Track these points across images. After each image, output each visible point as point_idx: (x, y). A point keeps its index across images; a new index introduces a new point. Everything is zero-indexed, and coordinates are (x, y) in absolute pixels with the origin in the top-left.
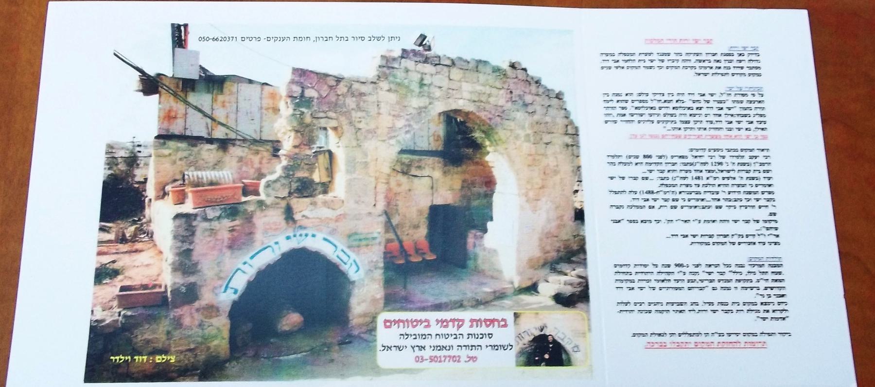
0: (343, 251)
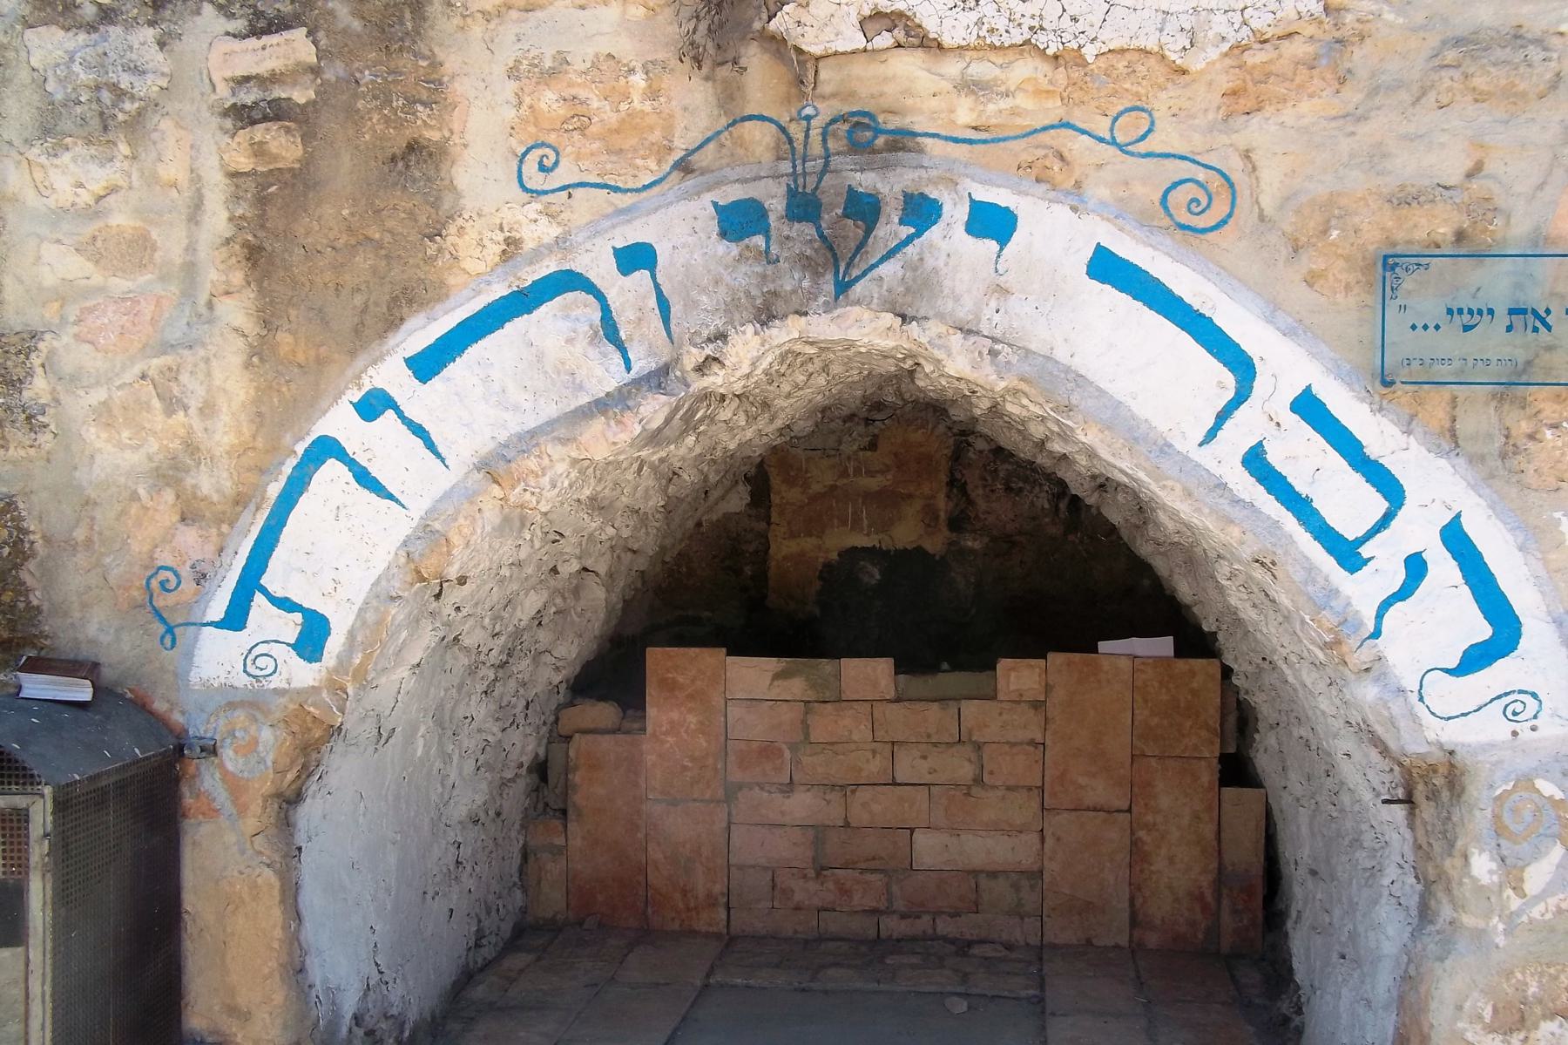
0: (1309, 407)
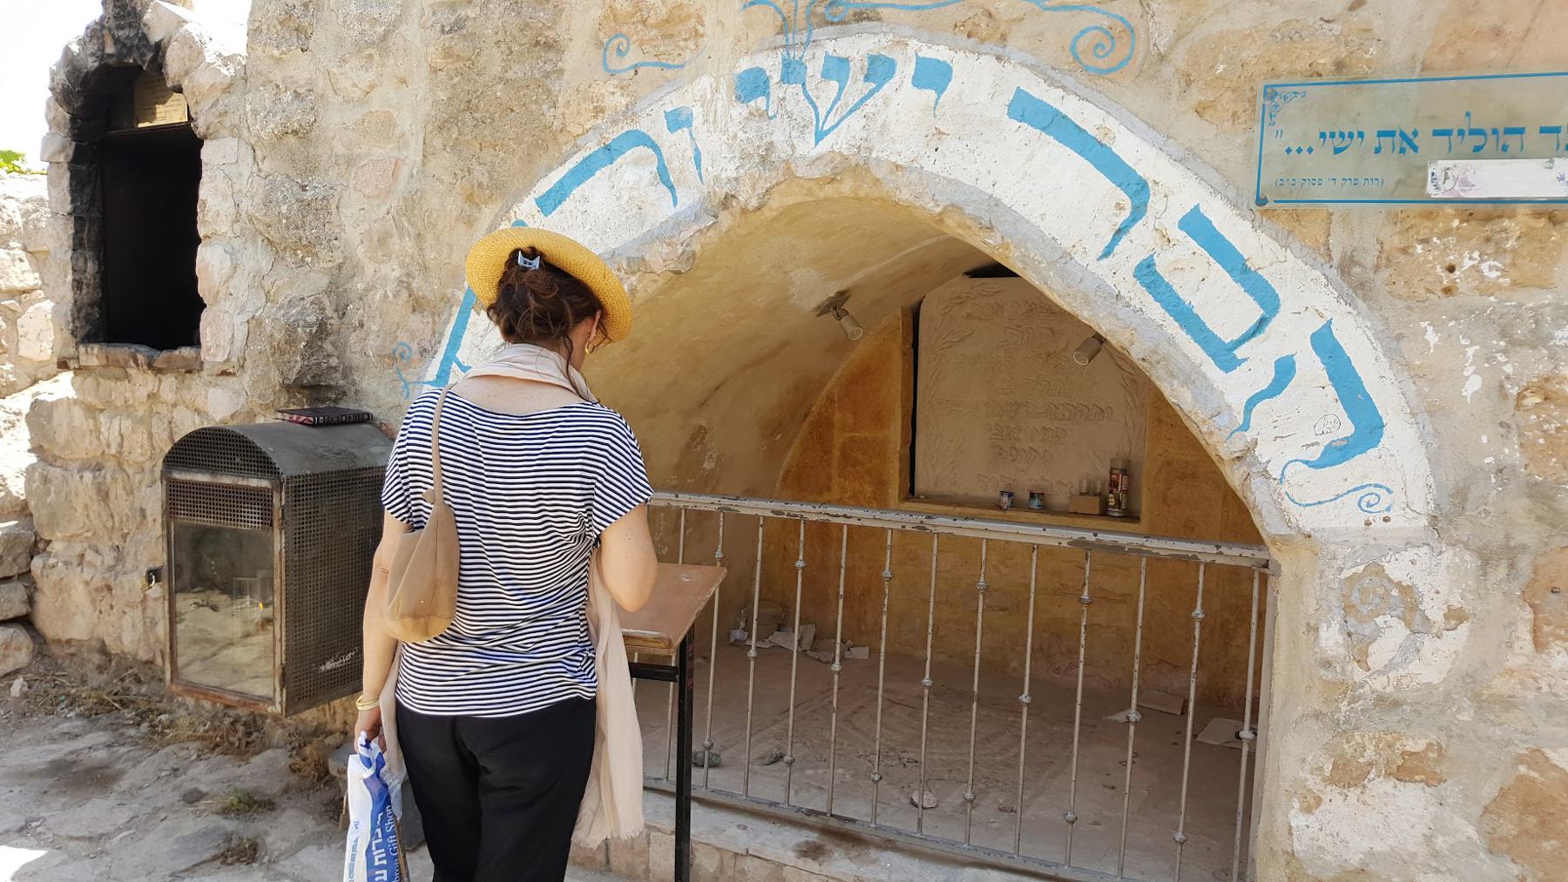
0: (1196, 225)
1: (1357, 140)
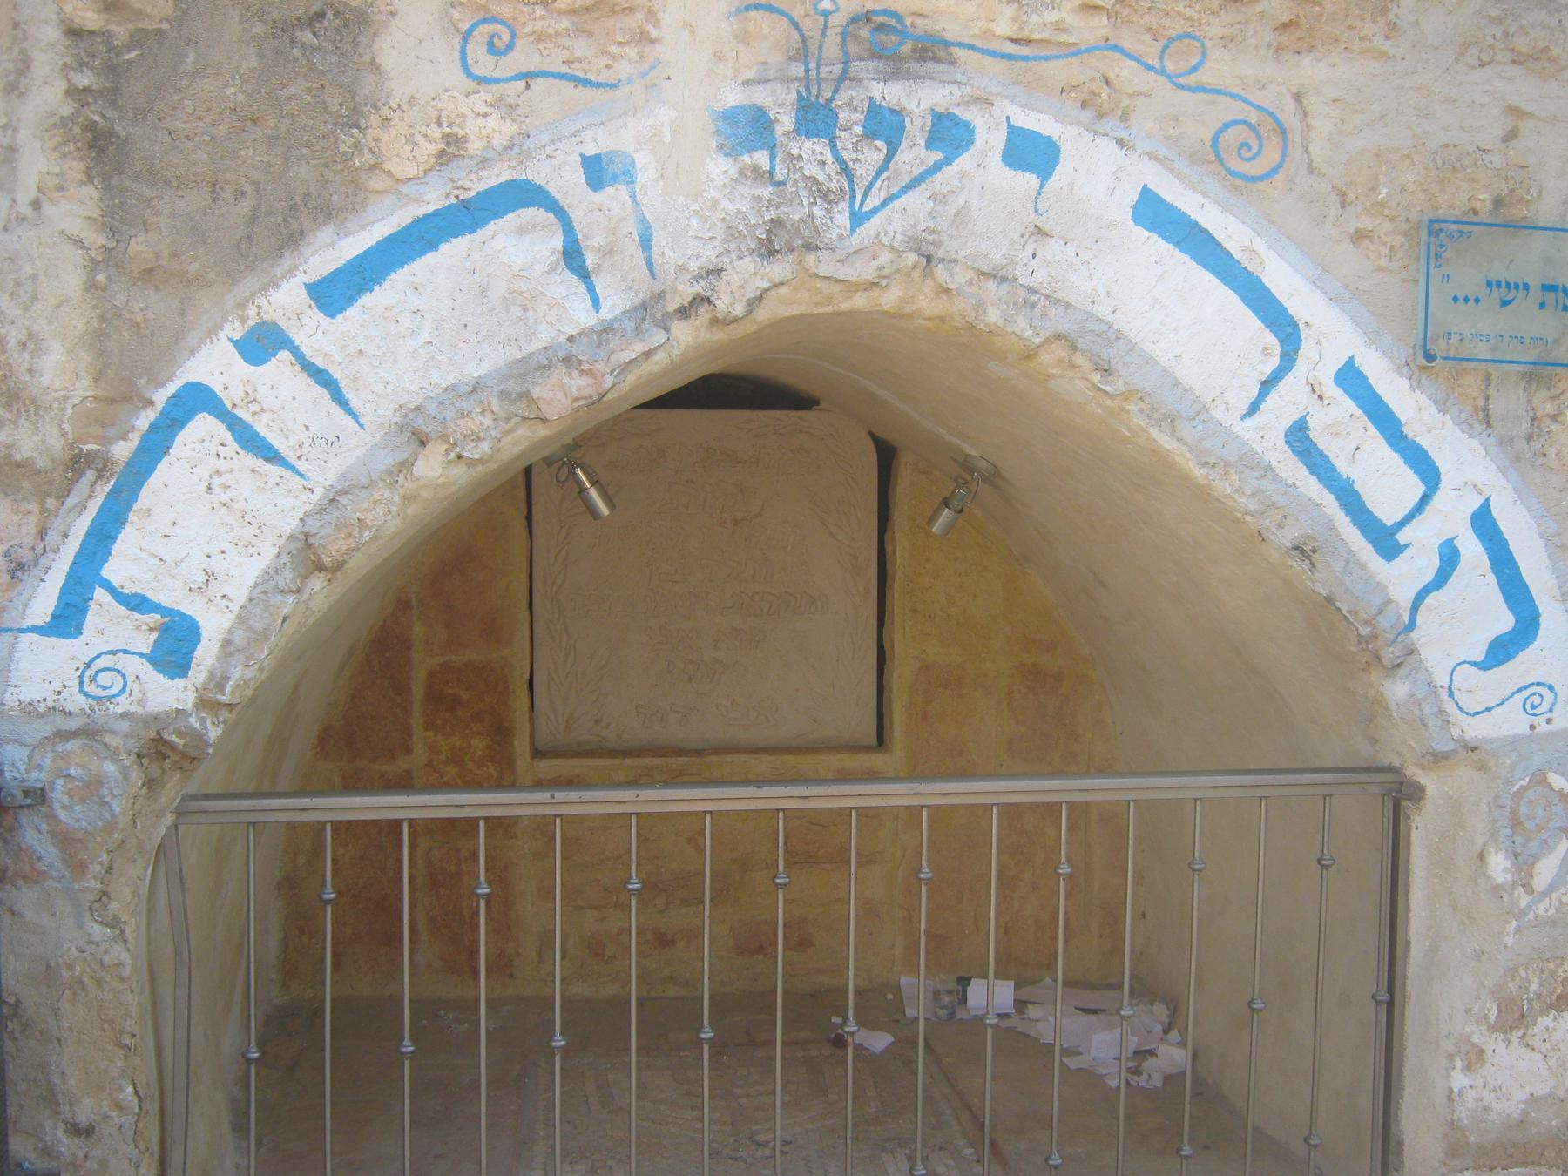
0: (1350, 377)
1: (1522, 293)
